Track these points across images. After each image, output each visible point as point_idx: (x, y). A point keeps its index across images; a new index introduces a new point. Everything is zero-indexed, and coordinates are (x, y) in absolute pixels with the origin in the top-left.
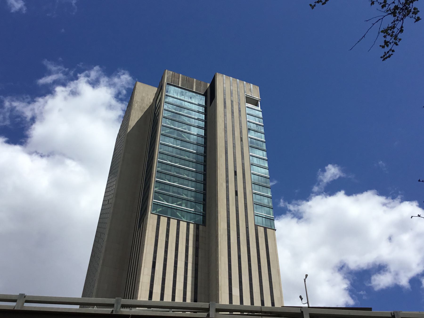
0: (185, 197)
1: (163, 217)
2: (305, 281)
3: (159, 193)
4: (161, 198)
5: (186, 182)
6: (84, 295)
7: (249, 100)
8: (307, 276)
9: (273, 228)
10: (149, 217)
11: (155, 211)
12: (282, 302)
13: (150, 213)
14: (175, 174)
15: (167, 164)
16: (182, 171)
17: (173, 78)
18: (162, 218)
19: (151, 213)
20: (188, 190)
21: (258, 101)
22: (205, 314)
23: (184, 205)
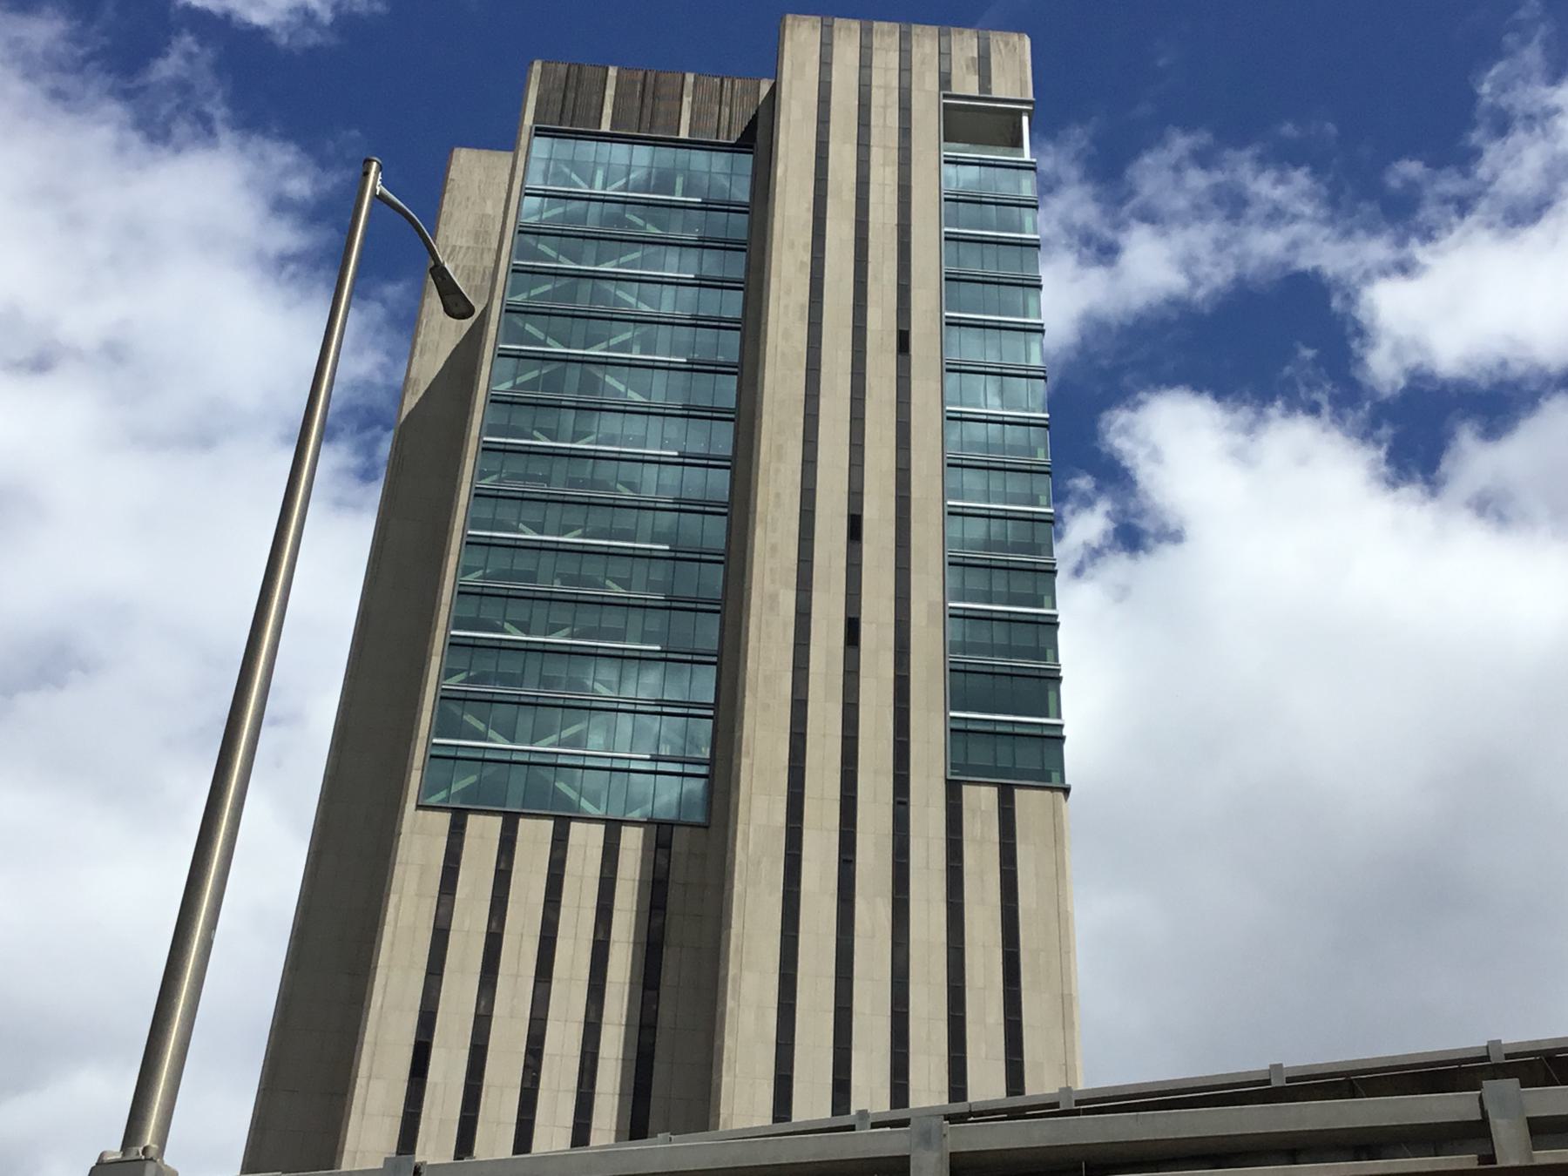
0: (616, 591)
1: (481, 818)
3: (464, 699)
5: (613, 619)
9: (1055, 783)
11: (443, 794)
12: (1067, 1068)
13: (410, 805)
14: (557, 587)
16: (592, 567)
17: (571, 95)
18: (473, 822)
19: (419, 807)
20: (634, 555)
21: (1020, 112)
23: (636, 348)
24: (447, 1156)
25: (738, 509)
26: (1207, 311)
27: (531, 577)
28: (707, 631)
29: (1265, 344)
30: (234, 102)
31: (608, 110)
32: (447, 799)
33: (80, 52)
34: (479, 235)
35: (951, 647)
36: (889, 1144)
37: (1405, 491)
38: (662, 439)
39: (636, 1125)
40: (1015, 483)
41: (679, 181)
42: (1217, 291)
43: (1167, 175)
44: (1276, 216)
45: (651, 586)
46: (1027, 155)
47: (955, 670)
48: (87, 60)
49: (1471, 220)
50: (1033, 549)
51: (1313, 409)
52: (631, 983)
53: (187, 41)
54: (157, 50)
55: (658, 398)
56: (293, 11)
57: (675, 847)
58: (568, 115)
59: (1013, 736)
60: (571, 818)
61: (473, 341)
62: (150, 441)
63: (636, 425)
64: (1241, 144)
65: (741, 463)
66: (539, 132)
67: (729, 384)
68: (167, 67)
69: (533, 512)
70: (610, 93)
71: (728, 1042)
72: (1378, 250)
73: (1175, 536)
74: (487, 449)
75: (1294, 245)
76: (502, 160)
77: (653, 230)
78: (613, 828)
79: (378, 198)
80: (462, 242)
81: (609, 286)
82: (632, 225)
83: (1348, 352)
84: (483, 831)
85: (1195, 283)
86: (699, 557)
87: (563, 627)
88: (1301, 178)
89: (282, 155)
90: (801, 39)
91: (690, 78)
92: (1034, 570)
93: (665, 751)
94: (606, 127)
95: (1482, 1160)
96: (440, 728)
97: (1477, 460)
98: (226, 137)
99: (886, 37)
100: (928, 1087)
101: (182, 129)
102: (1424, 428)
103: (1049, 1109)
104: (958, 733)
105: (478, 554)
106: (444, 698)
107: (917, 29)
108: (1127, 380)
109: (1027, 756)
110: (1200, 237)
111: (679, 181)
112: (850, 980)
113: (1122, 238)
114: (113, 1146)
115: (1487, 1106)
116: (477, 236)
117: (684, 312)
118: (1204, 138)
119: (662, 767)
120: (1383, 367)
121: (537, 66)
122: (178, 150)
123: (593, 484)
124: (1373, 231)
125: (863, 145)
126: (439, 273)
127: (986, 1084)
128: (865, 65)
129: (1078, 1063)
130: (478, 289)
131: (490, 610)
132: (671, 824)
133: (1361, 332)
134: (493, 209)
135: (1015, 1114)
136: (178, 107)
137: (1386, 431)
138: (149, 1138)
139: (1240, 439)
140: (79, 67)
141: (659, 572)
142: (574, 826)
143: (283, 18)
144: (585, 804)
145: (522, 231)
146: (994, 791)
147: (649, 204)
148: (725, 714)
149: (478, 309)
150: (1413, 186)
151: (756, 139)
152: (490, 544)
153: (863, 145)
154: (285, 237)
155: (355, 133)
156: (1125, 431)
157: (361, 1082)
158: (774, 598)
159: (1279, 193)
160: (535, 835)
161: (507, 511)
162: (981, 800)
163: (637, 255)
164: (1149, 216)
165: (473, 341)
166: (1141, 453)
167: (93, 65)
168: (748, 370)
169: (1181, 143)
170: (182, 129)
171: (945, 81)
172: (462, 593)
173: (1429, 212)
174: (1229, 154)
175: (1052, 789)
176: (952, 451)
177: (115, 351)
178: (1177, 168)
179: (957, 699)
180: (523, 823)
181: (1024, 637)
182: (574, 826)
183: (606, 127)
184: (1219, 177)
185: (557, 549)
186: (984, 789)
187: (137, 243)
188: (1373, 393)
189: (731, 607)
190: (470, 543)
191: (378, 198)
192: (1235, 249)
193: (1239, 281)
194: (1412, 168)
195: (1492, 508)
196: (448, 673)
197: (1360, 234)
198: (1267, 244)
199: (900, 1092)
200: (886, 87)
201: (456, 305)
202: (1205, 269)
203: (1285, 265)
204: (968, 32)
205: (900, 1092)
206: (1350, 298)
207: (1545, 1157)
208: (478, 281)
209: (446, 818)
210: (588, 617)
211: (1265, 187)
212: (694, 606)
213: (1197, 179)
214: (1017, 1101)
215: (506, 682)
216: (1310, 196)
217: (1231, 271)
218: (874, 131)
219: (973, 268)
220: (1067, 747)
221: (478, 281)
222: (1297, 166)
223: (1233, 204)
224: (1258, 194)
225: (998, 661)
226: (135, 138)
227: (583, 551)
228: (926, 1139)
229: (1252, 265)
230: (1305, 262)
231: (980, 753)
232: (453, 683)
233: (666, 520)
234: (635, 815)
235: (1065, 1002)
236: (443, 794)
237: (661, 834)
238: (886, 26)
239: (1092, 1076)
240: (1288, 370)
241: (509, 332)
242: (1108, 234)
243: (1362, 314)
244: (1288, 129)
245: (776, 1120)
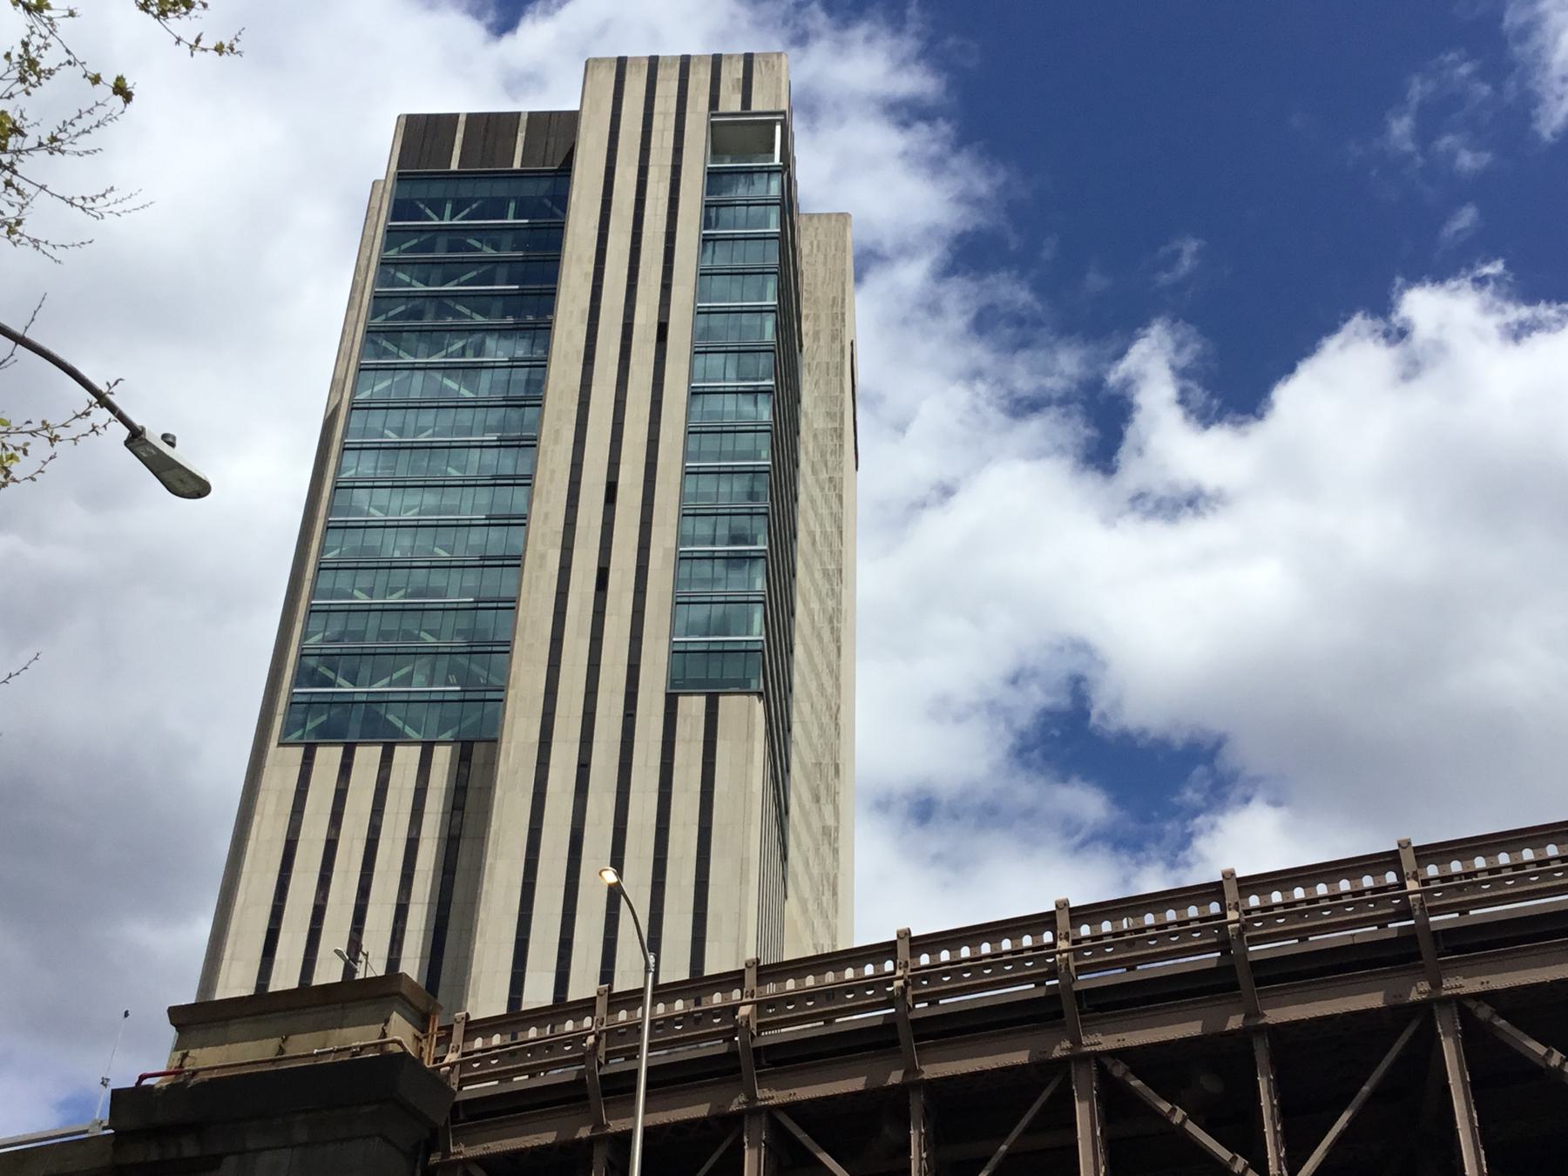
11: (299, 733)
13: (273, 743)
18: (322, 753)
19: (280, 744)
21: (773, 123)
23: (469, 352)
32: (301, 737)
57: (475, 759)
60: (718, 694)
63: (465, 416)
87: (398, 589)
144: (408, 730)
146: (703, 699)
147: (413, 263)
158: (543, 557)
162: (692, 708)
175: (748, 694)
176: (695, 421)
180: (359, 750)
186: (695, 698)
200: (665, 114)
236: (299, 733)
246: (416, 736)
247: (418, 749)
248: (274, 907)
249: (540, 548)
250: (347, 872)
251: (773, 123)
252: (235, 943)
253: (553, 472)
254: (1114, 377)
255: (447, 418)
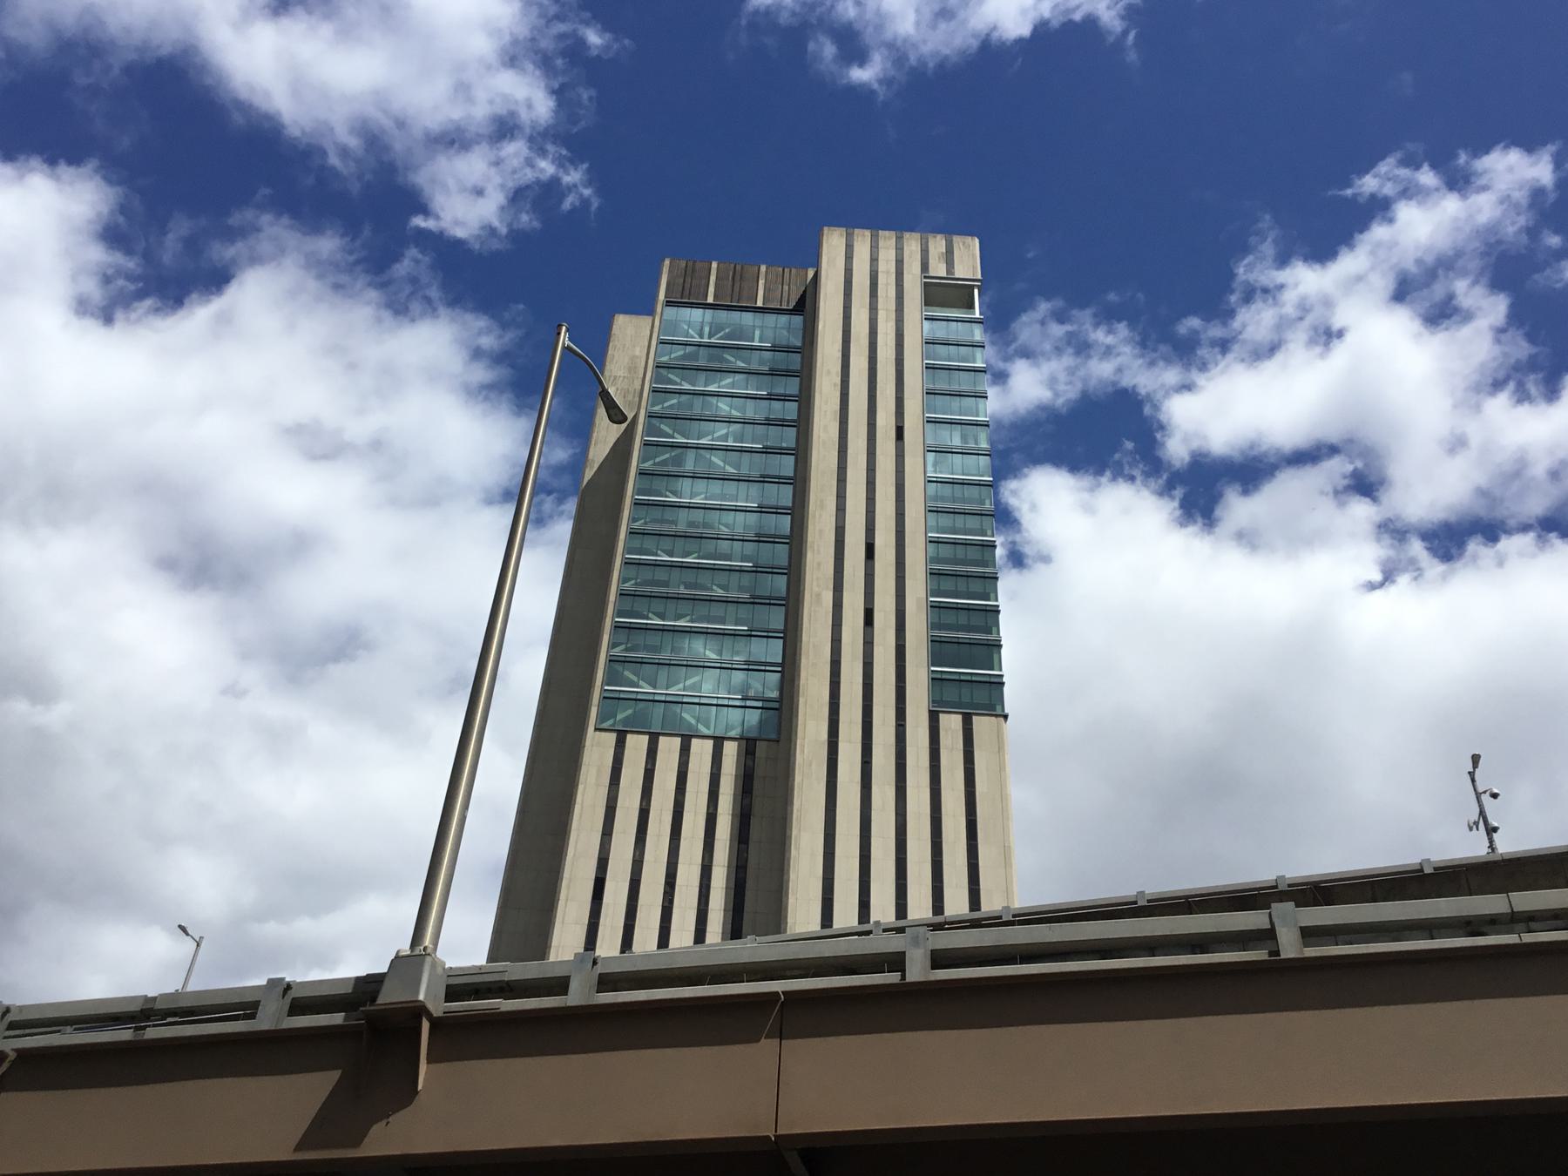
1: (635, 736)
2: (1473, 781)
3: (624, 661)
4: (632, 677)
5: (717, 610)
6: (491, 959)
7: (941, 294)
8: (1476, 759)
10: (588, 743)
11: (611, 722)
12: (1008, 892)
13: (591, 728)
14: (682, 590)
15: (656, 565)
16: (704, 578)
17: (688, 280)
18: (631, 739)
20: (731, 570)
21: (972, 287)
22: (892, 978)
24: (616, 952)
25: (796, 541)
26: (1064, 410)
27: (666, 584)
28: (776, 618)
29: (1104, 437)
30: (445, 287)
31: (711, 289)
33: (351, 258)
34: (632, 369)
35: (933, 626)
36: (893, 944)
37: (1191, 529)
38: (747, 497)
39: (735, 930)
40: (972, 522)
41: (757, 333)
42: (1069, 401)
43: (1037, 327)
44: (1108, 352)
45: (741, 589)
46: (977, 315)
47: (934, 641)
48: (358, 262)
49: (1230, 357)
50: (984, 564)
51: (1132, 479)
52: (222, 1076)
53: (413, 252)
54: (397, 258)
55: (745, 471)
56: (483, 228)
58: (736, 296)
59: (971, 682)
61: (627, 437)
62: (395, 502)
63: (731, 487)
64: (1082, 307)
65: (798, 511)
66: (669, 303)
67: (789, 461)
68: (402, 268)
69: (667, 543)
70: (713, 278)
71: (792, 876)
72: (1171, 376)
73: (1046, 559)
74: (637, 504)
75: (1119, 370)
76: (645, 321)
77: (740, 364)
78: (719, 742)
79: (567, 349)
80: (620, 373)
81: (714, 400)
82: (728, 361)
83: (1154, 440)
84: (637, 745)
85: (1057, 395)
86: (772, 571)
88: (1122, 329)
89: (481, 322)
90: (833, 243)
91: (714, 265)
92: (983, 577)
93: (752, 693)
94: (710, 300)
95: (1271, 954)
96: (611, 678)
97: (1239, 509)
98: (442, 310)
99: (887, 240)
100: (920, 907)
101: (416, 307)
102: (1205, 489)
103: (995, 921)
104: (936, 681)
105: (633, 570)
106: (612, 661)
107: (907, 235)
108: (1016, 457)
109: (981, 695)
110: (1056, 366)
111: (757, 333)
112: (869, 838)
113: (1008, 367)
114: (405, 946)
115: (1275, 920)
116: (630, 370)
117: (760, 416)
118: (1059, 303)
119: (749, 703)
120: (1176, 450)
121: (667, 262)
122: (413, 320)
123: (706, 525)
124: (1168, 361)
125: (873, 309)
126: (605, 395)
127: (956, 903)
128: (874, 260)
129: (1015, 889)
130: (630, 404)
131: (640, 605)
132: (755, 740)
133: (1162, 427)
134: (640, 352)
135: (975, 924)
136: (412, 293)
137: (1179, 492)
138: (427, 941)
139: (1086, 496)
140: (350, 269)
141: (746, 579)
142: (694, 741)
143: (476, 232)
145: (658, 366)
146: (959, 717)
148: (789, 669)
149: (630, 416)
150: (1195, 332)
151: (806, 306)
152: (639, 564)
153: (873, 309)
154: (481, 374)
155: (521, 306)
156: (1014, 493)
157: (561, 903)
158: (819, 595)
159: (1110, 340)
160: (669, 747)
161: (649, 543)
162: (951, 724)
163: (729, 380)
164: (1027, 354)
165: (627, 437)
166: (1025, 508)
167: (359, 268)
168: (801, 452)
169: (1044, 307)
170: (416, 307)
171: (925, 267)
172: (622, 594)
173: (1203, 352)
174: (1075, 312)
177: (377, 445)
178: (1043, 323)
179: (936, 658)
181: (977, 620)
182: (694, 741)
183: (710, 300)
184: (1068, 328)
185: (682, 566)
187: (390, 381)
188: (1170, 464)
189: (792, 603)
190: (627, 563)
191: (567, 349)
192: (1082, 373)
193: (1085, 395)
194: (1194, 322)
195: (1248, 539)
196: (613, 645)
197: (1161, 364)
198: (1101, 370)
199: (901, 910)
201: (616, 415)
202: (1061, 387)
203: (1114, 384)
204: (939, 237)
205: (901, 910)
206: (1156, 408)
207: (1312, 952)
208: (630, 397)
209: (613, 736)
210: (702, 609)
211: (1100, 336)
212: (769, 601)
213: (1057, 330)
214: (976, 915)
215: (647, 650)
216: (1127, 341)
217: (1079, 386)
218: (880, 300)
219: (941, 386)
220: (1006, 689)
221: (630, 397)
222: (1119, 321)
223: (1082, 348)
224: (1096, 341)
225: (961, 635)
226: (386, 314)
227: (698, 567)
228: (916, 942)
229: (1093, 383)
230: (1127, 381)
231: (950, 693)
232: (617, 651)
233: (750, 547)
234: (733, 734)
235: (1006, 852)
237: (749, 746)
238: (887, 233)
239: (1023, 899)
240: (1117, 456)
241: (649, 430)
242: (1001, 365)
243: (1163, 417)
244: (1112, 297)
245: (823, 926)
246: (705, 731)
247: (710, 743)
248: (864, 722)
249: (816, 589)
250: (659, 836)
251: (972, 287)
252: (569, 887)
253: (821, 531)
254: (528, 131)
255: (716, 487)
